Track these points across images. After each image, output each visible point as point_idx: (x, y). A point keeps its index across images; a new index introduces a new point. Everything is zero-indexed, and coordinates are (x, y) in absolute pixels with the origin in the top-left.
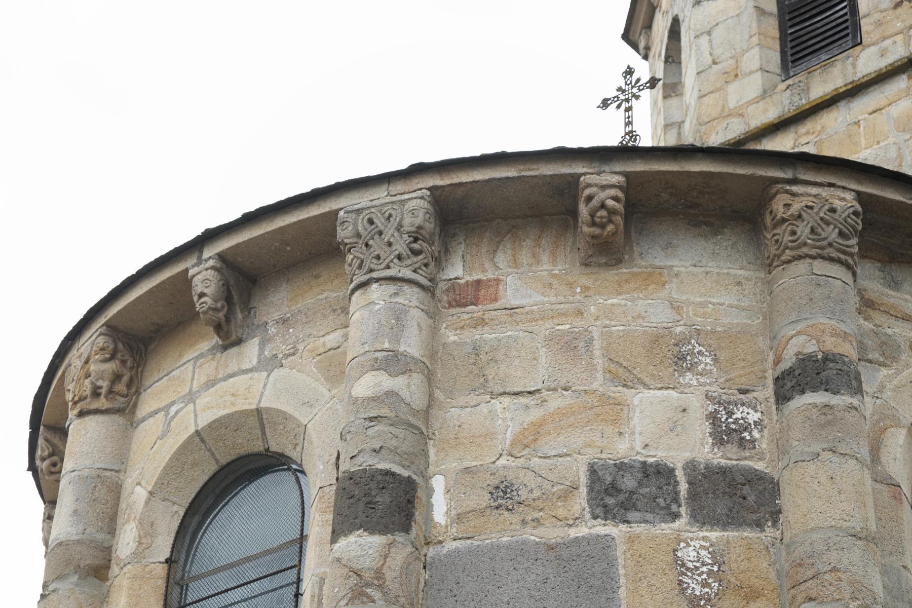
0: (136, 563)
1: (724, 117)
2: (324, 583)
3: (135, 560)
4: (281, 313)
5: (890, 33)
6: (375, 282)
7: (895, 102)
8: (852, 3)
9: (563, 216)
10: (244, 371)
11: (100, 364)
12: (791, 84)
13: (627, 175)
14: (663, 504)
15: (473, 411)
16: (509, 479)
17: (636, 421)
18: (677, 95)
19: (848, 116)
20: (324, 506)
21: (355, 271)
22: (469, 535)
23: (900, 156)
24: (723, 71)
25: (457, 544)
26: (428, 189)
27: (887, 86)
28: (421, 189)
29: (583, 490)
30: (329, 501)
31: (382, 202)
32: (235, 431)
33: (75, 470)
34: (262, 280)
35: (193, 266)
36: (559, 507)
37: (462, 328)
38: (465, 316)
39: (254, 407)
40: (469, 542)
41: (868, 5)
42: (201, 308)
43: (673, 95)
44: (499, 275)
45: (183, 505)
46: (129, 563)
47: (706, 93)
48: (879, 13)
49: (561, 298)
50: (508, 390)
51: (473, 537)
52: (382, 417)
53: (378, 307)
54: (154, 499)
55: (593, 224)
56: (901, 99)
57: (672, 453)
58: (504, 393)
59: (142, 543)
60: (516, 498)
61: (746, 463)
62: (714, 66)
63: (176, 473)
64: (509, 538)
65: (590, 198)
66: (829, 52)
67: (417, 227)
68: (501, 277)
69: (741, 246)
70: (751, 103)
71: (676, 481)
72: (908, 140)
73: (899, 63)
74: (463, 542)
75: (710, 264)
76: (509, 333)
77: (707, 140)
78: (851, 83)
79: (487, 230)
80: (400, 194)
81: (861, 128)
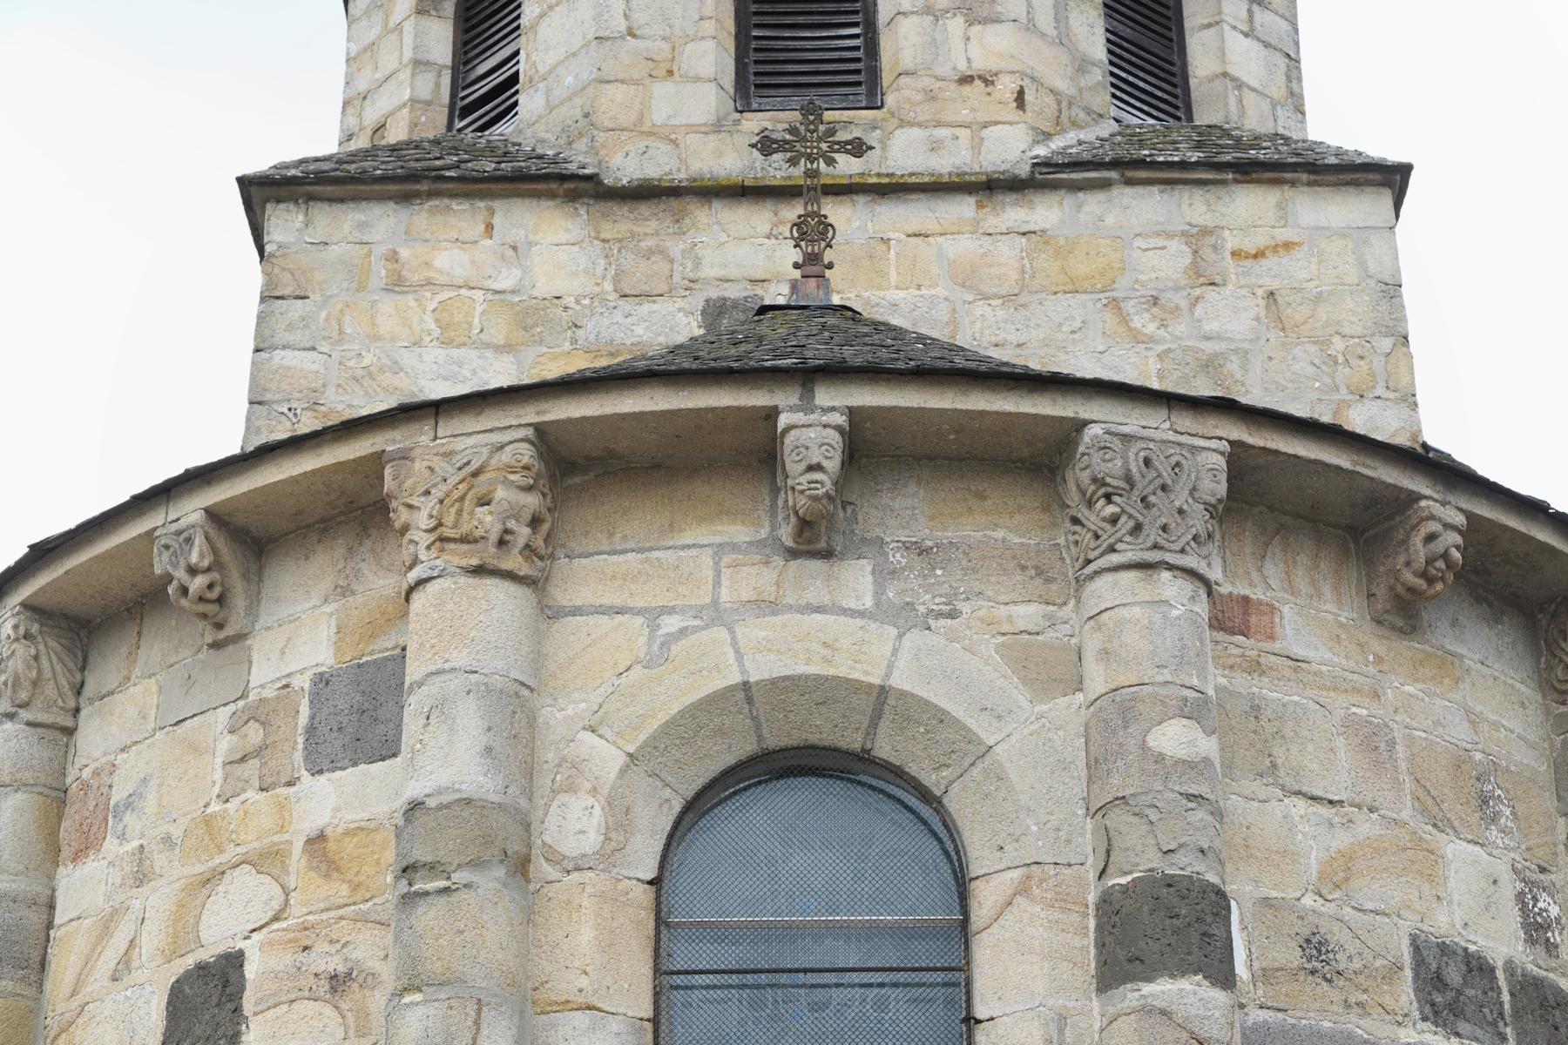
0: (603, 871)
1: (642, 133)
2: (1066, 1024)
3: (601, 866)
4: (912, 534)
5: (949, 119)
6: (1166, 569)
7: (952, 234)
8: (870, 35)
9: (1340, 532)
10: (845, 610)
11: (517, 491)
12: (770, 128)
13: (1469, 516)
14: (1489, 1018)
15: (1263, 808)
16: (1322, 931)
17: (1452, 884)
18: (440, 17)
19: (870, 224)
20: (1049, 896)
21: (1124, 535)
22: (1281, 1006)
23: (953, 322)
24: (645, 54)
25: (1264, 1015)
26: (1230, 442)
27: (939, 202)
28: (1220, 439)
29: (1408, 973)
30: (1057, 889)
31: (1164, 438)
32: (817, 704)
33: (476, 672)
34: (864, 460)
35: (792, 409)
36: (1385, 992)
37: (1232, 667)
38: (1236, 651)
39: (876, 681)
40: (1280, 1015)
41: (915, 58)
42: (809, 489)
43: (434, 13)
44: (1272, 598)
45: (680, 791)
46: (590, 868)
47: (612, 78)
48: (933, 80)
49: (1352, 664)
50: (1305, 789)
51: (1286, 1011)
52: (1203, 798)
53: (1175, 613)
54: (635, 768)
55: (1423, 575)
56: (963, 233)
57: (1491, 944)
58: (1298, 793)
59: (610, 839)
60: (1333, 963)
61: (1551, 975)
62: (629, 38)
63: (683, 738)
64: (1332, 1025)
65: (1431, 538)
66: (826, 99)
67: (1218, 500)
68: (1277, 604)
69: (1520, 647)
70: (692, 128)
71: (1498, 987)
72: (970, 303)
73: (973, 178)
74: (1271, 1013)
75: (1496, 666)
76: (1295, 698)
77: (607, 159)
78: (887, 175)
79: (1248, 518)
80: (1189, 434)
81: (892, 251)
